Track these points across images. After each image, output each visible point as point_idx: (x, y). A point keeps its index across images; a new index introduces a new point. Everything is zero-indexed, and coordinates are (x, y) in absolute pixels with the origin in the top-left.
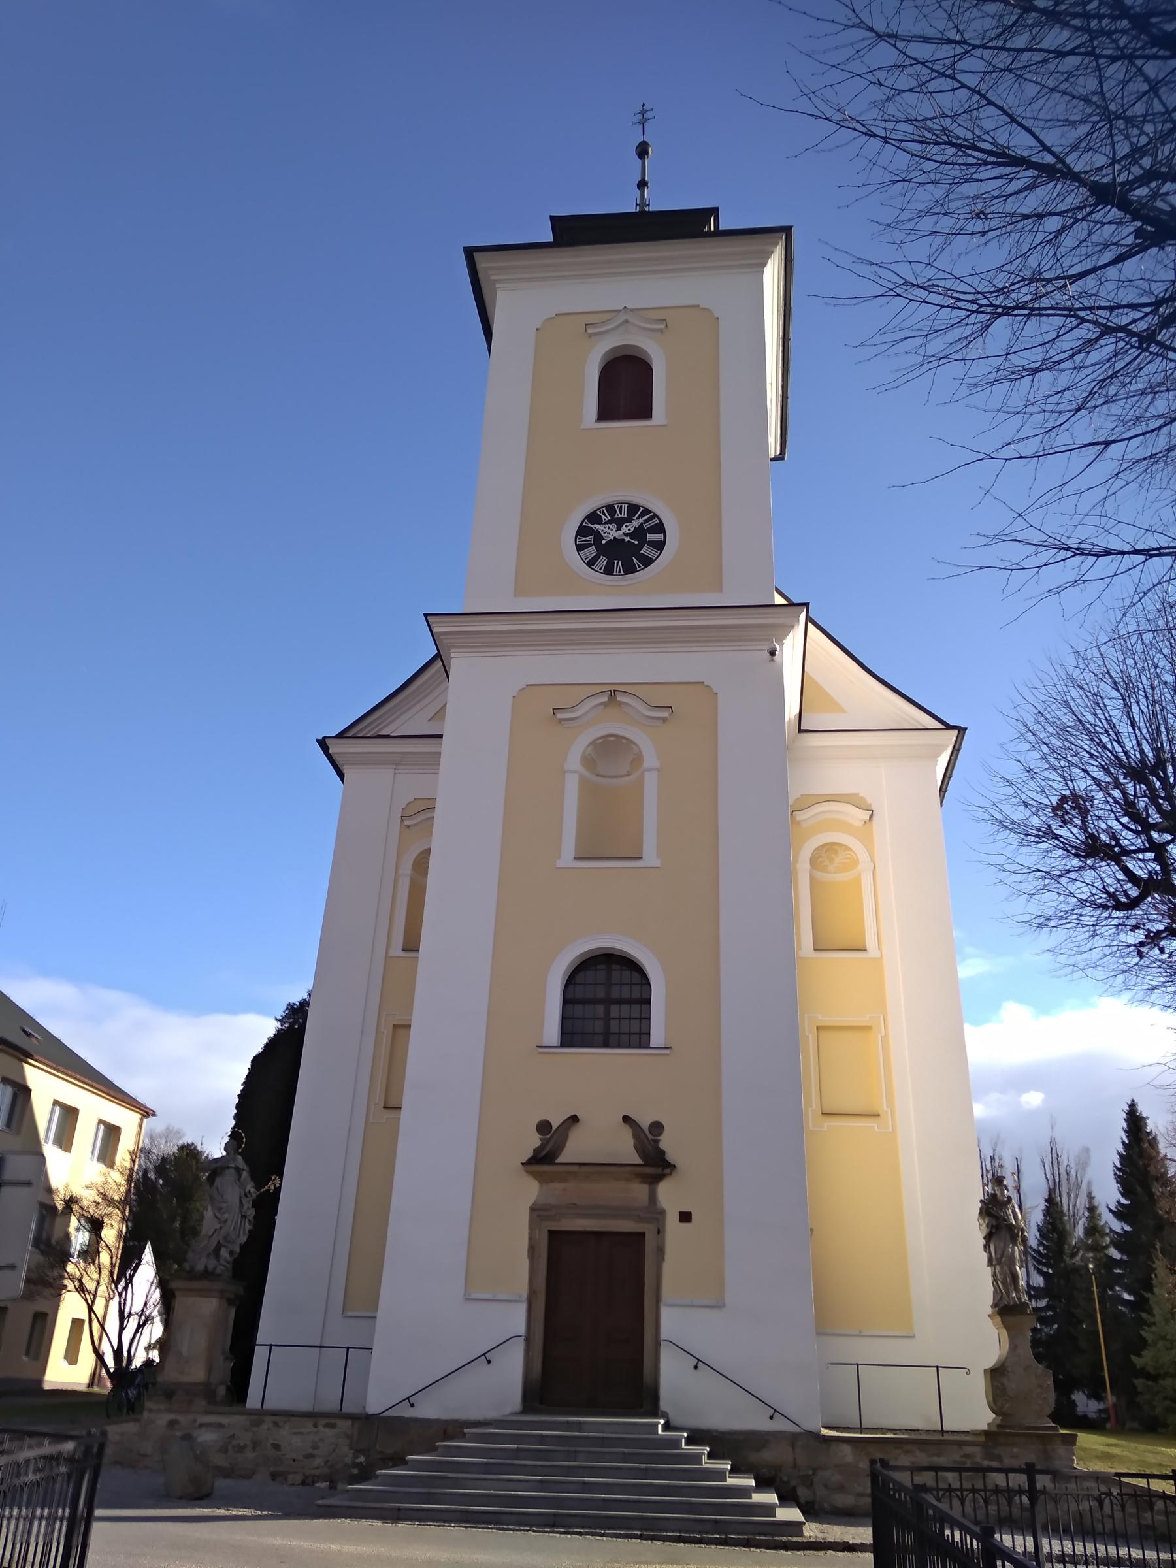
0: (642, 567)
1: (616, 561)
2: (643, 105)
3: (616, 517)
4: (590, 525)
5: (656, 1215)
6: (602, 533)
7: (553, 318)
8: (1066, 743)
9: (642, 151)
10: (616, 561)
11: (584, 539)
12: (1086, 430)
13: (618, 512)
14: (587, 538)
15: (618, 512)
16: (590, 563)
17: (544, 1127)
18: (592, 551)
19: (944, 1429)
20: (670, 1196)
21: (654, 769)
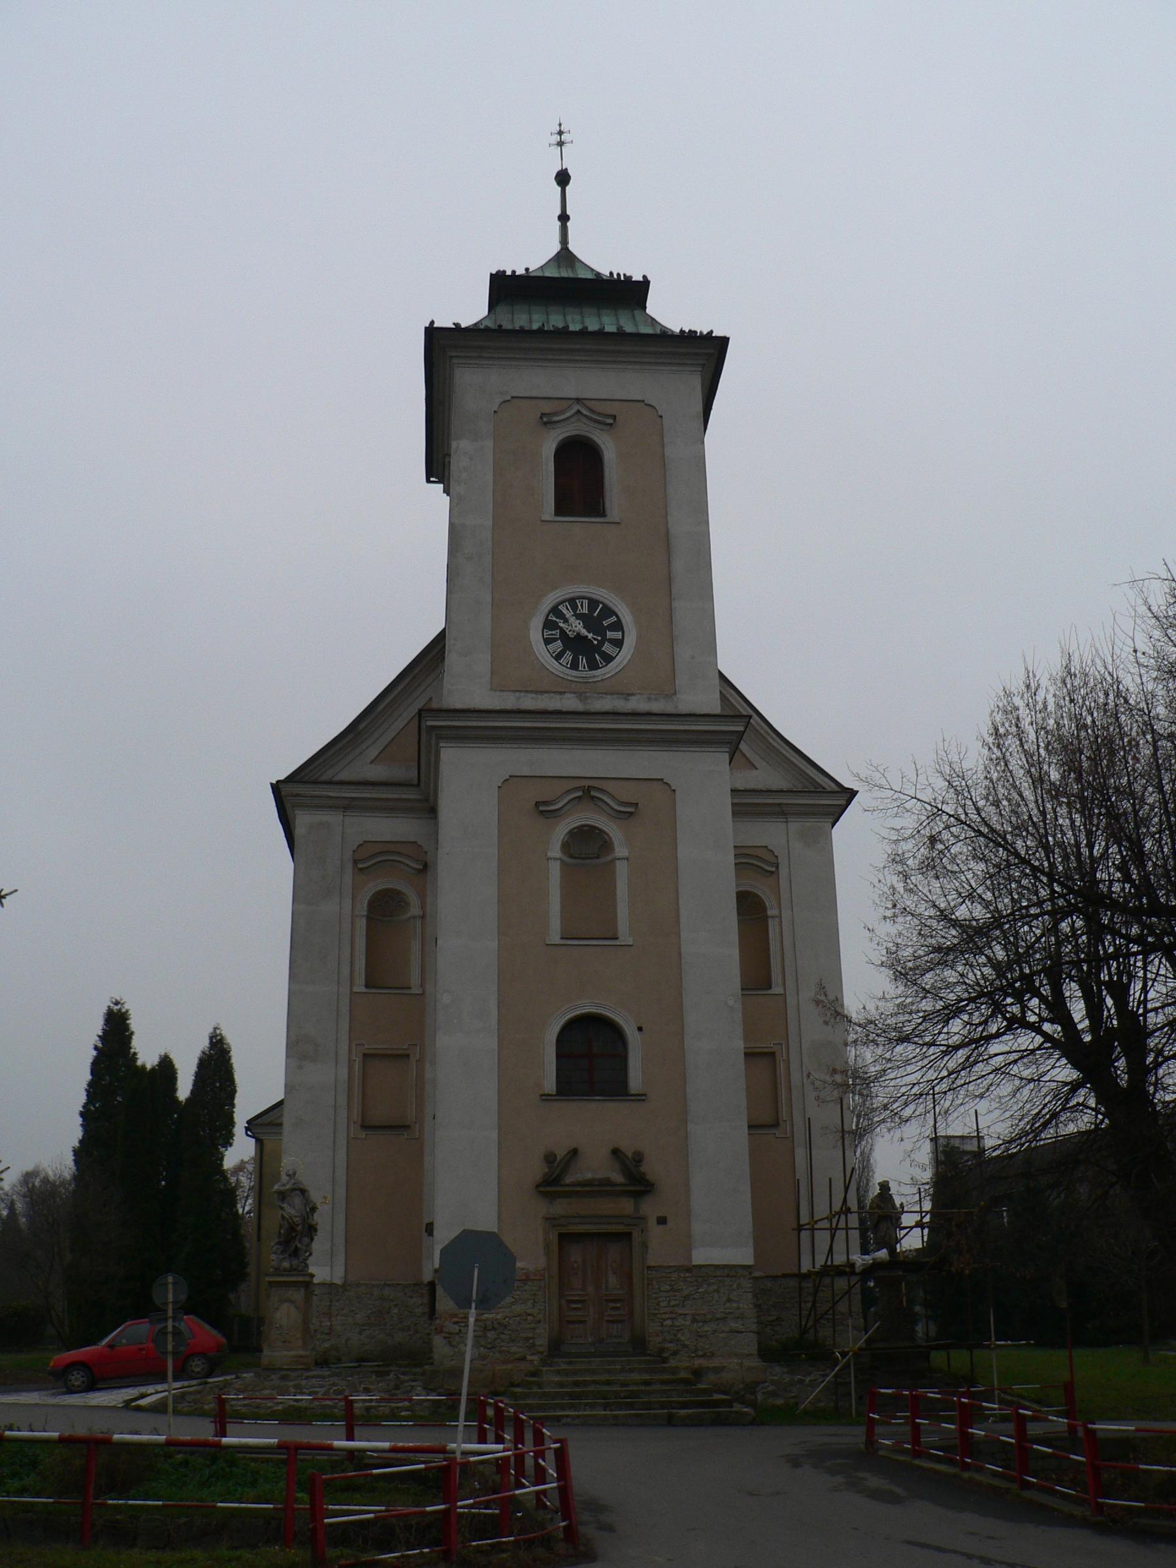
0: (604, 664)
1: (581, 657)
2: (560, 125)
3: (578, 612)
4: (554, 619)
5: (639, 1220)
6: (567, 631)
7: (509, 401)
8: (960, 811)
9: (563, 178)
10: (581, 657)
11: (550, 632)
12: (572, 142)
13: (580, 607)
14: (553, 632)
15: (580, 607)
16: (558, 657)
17: (550, 1158)
18: (558, 646)
19: (816, 1232)
20: (650, 1209)
21: (624, 859)
